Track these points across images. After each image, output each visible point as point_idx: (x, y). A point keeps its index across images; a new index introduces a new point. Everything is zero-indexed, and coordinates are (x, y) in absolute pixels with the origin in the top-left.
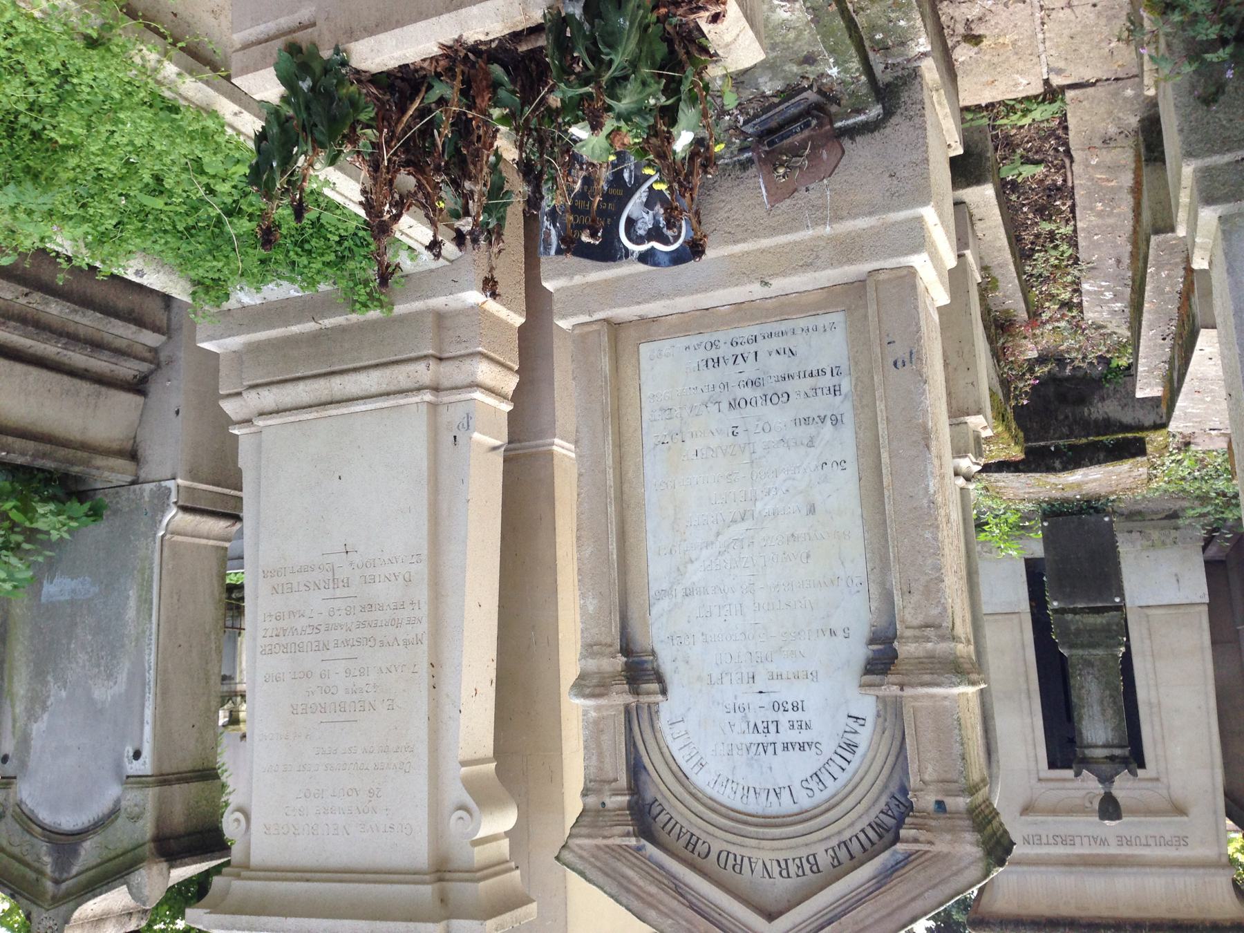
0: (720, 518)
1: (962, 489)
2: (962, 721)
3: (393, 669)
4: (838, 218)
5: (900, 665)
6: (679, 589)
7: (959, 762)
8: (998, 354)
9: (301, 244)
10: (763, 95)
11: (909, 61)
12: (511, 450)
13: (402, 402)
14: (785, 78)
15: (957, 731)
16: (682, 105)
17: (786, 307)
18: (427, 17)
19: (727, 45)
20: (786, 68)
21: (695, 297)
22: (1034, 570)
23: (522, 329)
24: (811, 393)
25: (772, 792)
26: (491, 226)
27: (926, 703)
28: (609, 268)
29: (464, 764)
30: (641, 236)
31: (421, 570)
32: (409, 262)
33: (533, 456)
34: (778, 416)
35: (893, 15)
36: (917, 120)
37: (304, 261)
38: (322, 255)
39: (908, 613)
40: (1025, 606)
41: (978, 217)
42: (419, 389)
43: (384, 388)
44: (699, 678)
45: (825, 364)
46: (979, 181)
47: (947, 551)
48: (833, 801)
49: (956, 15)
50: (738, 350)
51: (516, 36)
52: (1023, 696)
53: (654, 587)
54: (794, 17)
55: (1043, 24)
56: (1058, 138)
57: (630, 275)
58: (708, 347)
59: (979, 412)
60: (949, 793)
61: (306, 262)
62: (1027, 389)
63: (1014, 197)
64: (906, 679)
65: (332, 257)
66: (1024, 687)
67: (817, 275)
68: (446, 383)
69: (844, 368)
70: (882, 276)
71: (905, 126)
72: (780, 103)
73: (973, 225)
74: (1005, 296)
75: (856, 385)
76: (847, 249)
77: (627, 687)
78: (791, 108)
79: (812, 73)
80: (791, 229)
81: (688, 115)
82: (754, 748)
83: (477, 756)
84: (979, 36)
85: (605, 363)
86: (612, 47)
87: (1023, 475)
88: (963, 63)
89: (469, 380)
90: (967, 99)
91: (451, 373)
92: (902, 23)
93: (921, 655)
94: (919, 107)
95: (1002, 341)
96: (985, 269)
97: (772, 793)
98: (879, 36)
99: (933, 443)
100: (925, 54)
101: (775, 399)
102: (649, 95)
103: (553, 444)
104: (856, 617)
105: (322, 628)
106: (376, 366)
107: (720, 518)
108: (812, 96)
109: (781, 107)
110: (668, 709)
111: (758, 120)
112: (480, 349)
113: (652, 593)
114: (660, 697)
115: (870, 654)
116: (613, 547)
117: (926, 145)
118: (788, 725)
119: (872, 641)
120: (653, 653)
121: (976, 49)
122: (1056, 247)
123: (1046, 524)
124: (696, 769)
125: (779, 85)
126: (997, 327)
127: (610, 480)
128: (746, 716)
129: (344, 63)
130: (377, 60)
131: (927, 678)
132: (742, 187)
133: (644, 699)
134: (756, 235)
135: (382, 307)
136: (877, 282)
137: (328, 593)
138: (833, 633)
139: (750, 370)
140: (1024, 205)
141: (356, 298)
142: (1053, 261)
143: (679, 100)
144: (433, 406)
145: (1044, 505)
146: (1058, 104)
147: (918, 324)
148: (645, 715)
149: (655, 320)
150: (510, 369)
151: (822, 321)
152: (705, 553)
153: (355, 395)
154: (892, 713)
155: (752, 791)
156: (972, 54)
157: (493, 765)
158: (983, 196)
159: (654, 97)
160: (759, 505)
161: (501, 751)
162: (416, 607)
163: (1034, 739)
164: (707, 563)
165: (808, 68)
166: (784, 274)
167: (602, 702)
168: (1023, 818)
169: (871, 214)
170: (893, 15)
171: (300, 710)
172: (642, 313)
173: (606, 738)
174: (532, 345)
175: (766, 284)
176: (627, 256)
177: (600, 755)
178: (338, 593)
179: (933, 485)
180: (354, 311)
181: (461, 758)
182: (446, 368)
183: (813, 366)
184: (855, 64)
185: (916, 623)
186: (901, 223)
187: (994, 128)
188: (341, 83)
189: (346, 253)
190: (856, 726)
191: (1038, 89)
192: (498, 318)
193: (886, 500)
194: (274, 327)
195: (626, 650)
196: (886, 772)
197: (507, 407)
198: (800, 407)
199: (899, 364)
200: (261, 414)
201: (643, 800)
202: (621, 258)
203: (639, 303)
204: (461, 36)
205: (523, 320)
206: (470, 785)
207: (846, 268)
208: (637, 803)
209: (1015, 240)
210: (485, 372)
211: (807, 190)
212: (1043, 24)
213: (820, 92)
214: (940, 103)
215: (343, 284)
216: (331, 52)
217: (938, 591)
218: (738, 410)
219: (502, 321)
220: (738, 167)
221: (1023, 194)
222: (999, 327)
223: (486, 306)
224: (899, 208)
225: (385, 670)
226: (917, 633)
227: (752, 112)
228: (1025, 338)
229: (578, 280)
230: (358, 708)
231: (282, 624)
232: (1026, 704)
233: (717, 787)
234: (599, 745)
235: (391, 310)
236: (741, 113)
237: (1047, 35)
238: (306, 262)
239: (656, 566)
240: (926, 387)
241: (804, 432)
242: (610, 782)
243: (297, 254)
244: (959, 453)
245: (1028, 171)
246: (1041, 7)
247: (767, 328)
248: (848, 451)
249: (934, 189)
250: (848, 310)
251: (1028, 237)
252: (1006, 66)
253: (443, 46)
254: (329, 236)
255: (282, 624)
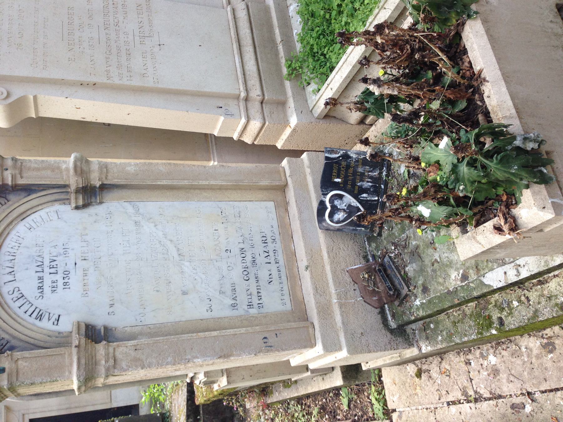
0: (180, 242)
1: (187, 375)
2: (55, 383)
3: (92, 63)
4: (341, 306)
5: (91, 345)
6: (139, 218)
7: (28, 381)
8: (250, 390)
9: (323, 33)
10: (405, 266)
11: (417, 341)
12: (211, 138)
13: (240, 81)
14: (415, 277)
15: (49, 380)
16: (451, 208)
17: (293, 278)
18: (498, 63)
19: (474, 238)
20: (421, 278)
21: (300, 231)
22: (132, 409)
23: (275, 147)
24: (249, 292)
25: (12, 270)
26: (366, 104)
27: (67, 361)
28: (315, 187)
29: (35, 98)
30: (333, 202)
31: (149, 83)
32: (311, 89)
33: (208, 151)
34: (236, 275)
35: (444, 333)
36: (389, 346)
37: (314, 35)
38: (317, 44)
39: (123, 350)
40: (115, 405)
41: (325, 378)
42: (247, 90)
43: (247, 73)
44: (85, 229)
45: (264, 300)
46: (345, 378)
47: (159, 370)
48: (6, 306)
49: (433, 365)
50: (271, 254)
51: (487, 114)
52: (68, 406)
53: (141, 205)
54: (451, 281)
55: (427, 409)
56: (362, 416)
57: (310, 198)
58: (273, 238)
59: (229, 383)
60: (10, 375)
61: (313, 36)
62: (231, 404)
63: (331, 394)
64: (82, 348)
65: (315, 50)
66: (73, 406)
67: (312, 295)
68: (249, 105)
69: (262, 310)
70: (311, 330)
71: (386, 340)
72: (401, 275)
73: (321, 375)
74: (280, 391)
75: (253, 317)
76: (325, 311)
77: (81, 186)
78: (398, 281)
79: (417, 291)
80: (335, 281)
81: (442, 212)
82: (40, 259)
83: (39, 106)
84: (421, 377)
85: (265, 183)
86: (501, 162)
87: (185, 403)
88: (406, 368)
89: (251, 117)
90: (384, 372)
91: (255, 107)
92: (440, 338)
93: (98, 358)
94: (395, 347)
95: (257, 391)
96: (296, 382)
97: (11, 270)
98: (432, 326)
99: (221, 360)
100: (420, 350)
101: (245, 273)
102: (466, 186)
103: (214, 161)
104: (121, 320)
105: (117, 28)
106: (259, 70)
107: (180, 242)
108: (405, 291)
109: (399, 276)
110: (66, 210)
111: (391, 264)
112: (267, 123)
113: (138, 203)
114: (73, 205)
115: (98, 327)
116: (164, 182)
117: (377, 351)
118: (55, 280)
119: (106, 328)
120: (101, 203)
121: (414, 375)
122: (303, 416)
123: (158, 415)
124: (28, 226)
125: (410, 274)
126: (263, 388)
127: (201, 183)
128: (60, 255)
129: (469, 16)
130: (471, 35)
131: (83, 361)
132: (355, 256)
133: (73, 196)
134: (332, 263)
135: (289, 75)
136: (308, 327)
137: (137, 33)
138: (112, 305)
139: (261, 260)
140: (326, 400)
141: (294, 62)
142: (296, 415)
143: (453, 206)
144: (238, 97)
145: (168, 414)
146: (382, 416)
147: (286, 350)
148: (63, 196)
149: (287, 210)
150: (255, 139)
151: (287, 298)
152: (160, 234)
153: (243, 58)
154: (61, 341)
155: (13, 258)
156: (410, 373)
157: (34, 116)
158: (337, 380)
159: (464, 189)
160: (187, 264)
161: (44, 123)
162: (128, 78)
163: (45, 412)
164: (154, 234)
165: (420, 290)
166: (312, 278)
167: (72, 172)
168: (3, 407)
169: (343, 323)
170: (444, 333)
171: (70, 11)
172: (291, 203)
173: (49, 173)
174: (268, 152)
175: (307, 268)
176: (323, 194)
177: (38, 169)
178: (137, 38)
179: (199, 361)
180: (286, 61)
181: (39, 96)
182: (257, 105)
183: (263, 294)
184: (421, 313)
185: (117, 354)
186: (339, 340)
187: (369, 384)
188: (458, 14)
189: (316, 58)
190: (53, 320)
191: (390, 406)
192: (281, 134)
193: (190, 335)
194: (278, 20)
195: (104, 187)
196: (23, 337)
197: (235, 137)
198: (241, 286)
199: (265, 340)
200: (234, 10)
201: (9, 193)
202: (322, 191)
203: (296, 202)
204: (488, 82)
205: (279, 147)
206: (21, 102)
207: (315, 311)
208: (7, 190)
209: (308, 396)
210: (255, 125)
211: (354, 290)
212: (427, 409)
213: (407, 295)
214: (392, 358)
215: (301, 55)
216: (475, 10)
217: (136, 366)
218: (239, 253)
219: (280, 136)
220: (365, 254)
221: (333, 399)
222: (264, 390)
223: (288, 128)
224: (346, 338)
225: (92, 58)
226: (111, 355)
227: (396, 260)
228: (258, 403)
229: (308, 171)
230: (70, 42)
231: (120, 7)
232: (64, 407)
233: (16, 238)
234: (44, 169)
235: (287, 79)
236: (395, 255)
237: (420, 411)
238: (313, 36)
239: (152, 206)
240: (253, 355)
241: (228, 288)
242: (20, 174)
243: (318, 31)
244: (206, 374)
245: (345, 401)
246: (437, 408)
247: (283, 270)
248: (216, 314)
249: (354, 356)
250: (292, 312)
251: (308, 402)
252: (404, 390)
253: (480, 72)
254: (327, 48)
255: (120, 7)
